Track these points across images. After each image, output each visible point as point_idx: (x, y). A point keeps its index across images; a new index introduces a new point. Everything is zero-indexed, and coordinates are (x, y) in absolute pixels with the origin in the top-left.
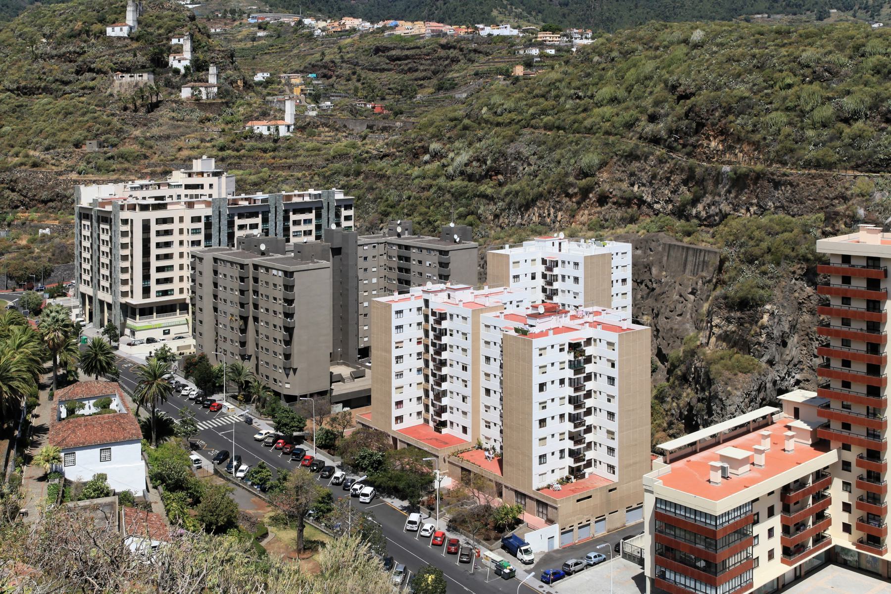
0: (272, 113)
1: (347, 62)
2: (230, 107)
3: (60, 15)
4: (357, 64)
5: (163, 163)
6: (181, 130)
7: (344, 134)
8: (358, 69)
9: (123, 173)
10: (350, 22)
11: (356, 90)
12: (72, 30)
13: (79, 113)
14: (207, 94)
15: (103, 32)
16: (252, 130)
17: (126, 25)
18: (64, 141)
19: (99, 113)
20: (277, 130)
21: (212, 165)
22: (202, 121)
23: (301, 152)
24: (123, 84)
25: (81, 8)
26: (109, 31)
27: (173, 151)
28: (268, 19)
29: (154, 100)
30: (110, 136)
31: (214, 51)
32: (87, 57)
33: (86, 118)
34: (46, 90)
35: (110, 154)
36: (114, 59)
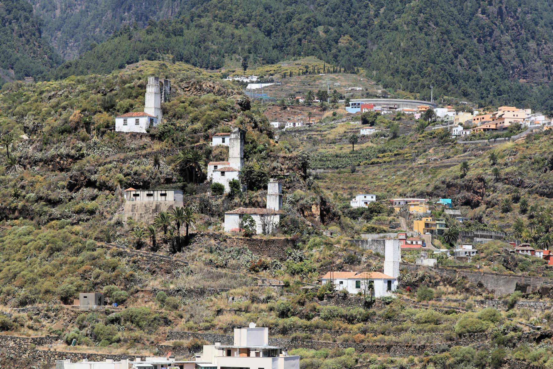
0: (363, 259)
1: (506, 180)
2: (298, 248)
3: (50, 98)
4: (521, 184)
5: (193, 332)
6: (222, 281)
7: (479, 298)
8: (522, 192)
9: (132, 346)
10: (511, 115)
11: (519, 228)
12: (66, 121)
13: (71, 249)
14: (264, 225)
15: (110, 126)
16: (331, 287)
17: (144, 115)
18: (47, 292)
19: (99, 251)
20: (371, 287)
21: (263, 339)
22: (254, 269)
23: (408, 324)
24: (138, 207)
25: (80, 87)
26: (120, 124)
27: (210, 313)
28: (378, 108)
29: (183, 232)
30: (112, 288)
31: (276, 158)
32: (86, 164)
33: (80, 258)
34: (25, 213)
35: (113, 316)
36: (125, 167)
